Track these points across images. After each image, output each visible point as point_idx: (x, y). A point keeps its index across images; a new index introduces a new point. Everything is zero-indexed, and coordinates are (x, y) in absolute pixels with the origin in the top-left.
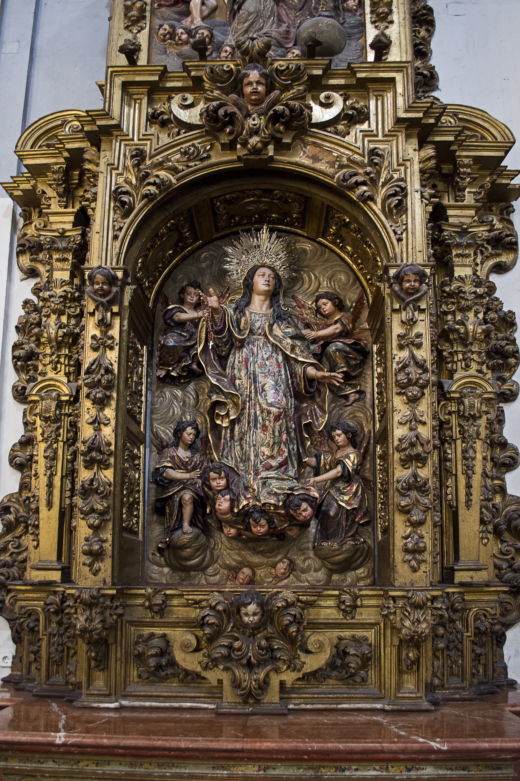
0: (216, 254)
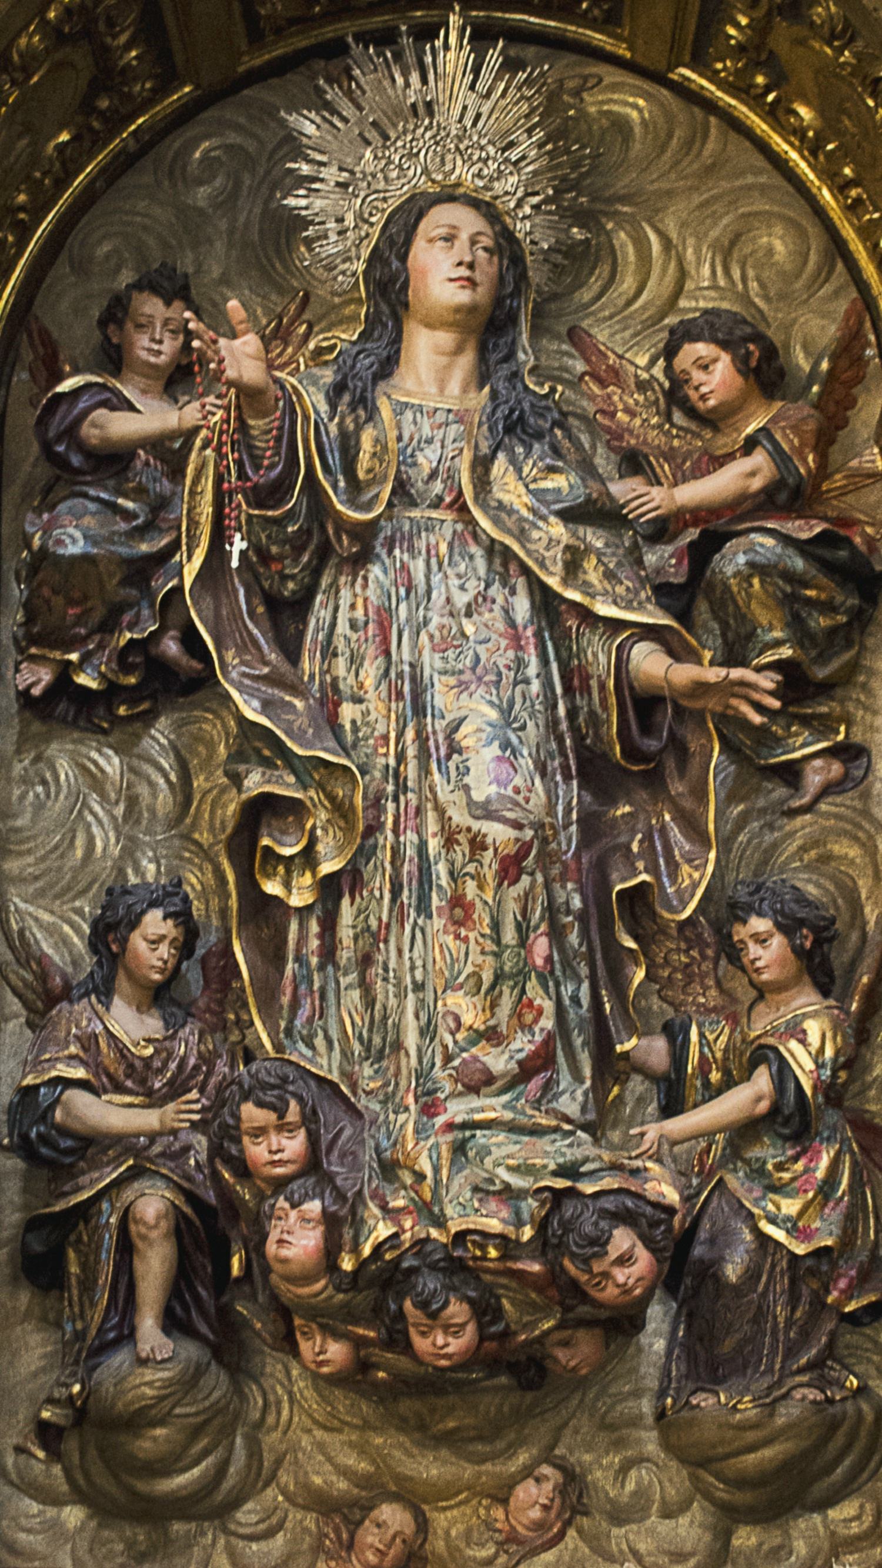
0: (251, 146)
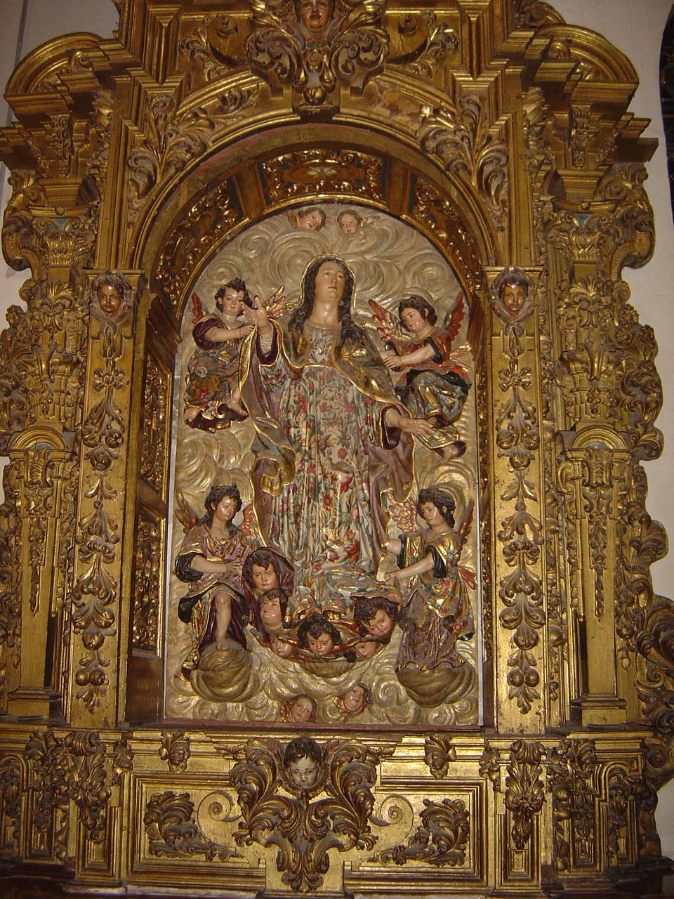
0: (267, 238)
